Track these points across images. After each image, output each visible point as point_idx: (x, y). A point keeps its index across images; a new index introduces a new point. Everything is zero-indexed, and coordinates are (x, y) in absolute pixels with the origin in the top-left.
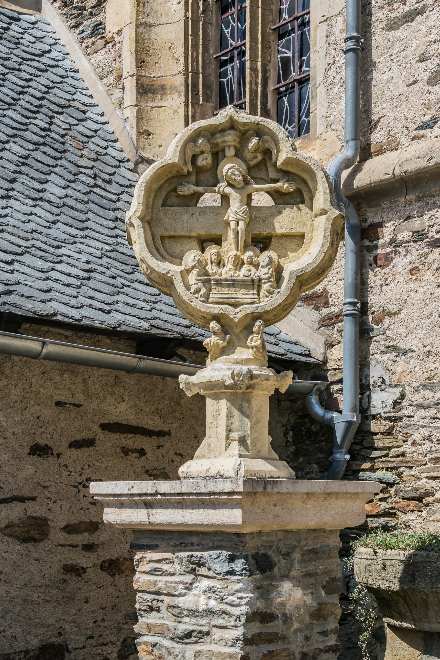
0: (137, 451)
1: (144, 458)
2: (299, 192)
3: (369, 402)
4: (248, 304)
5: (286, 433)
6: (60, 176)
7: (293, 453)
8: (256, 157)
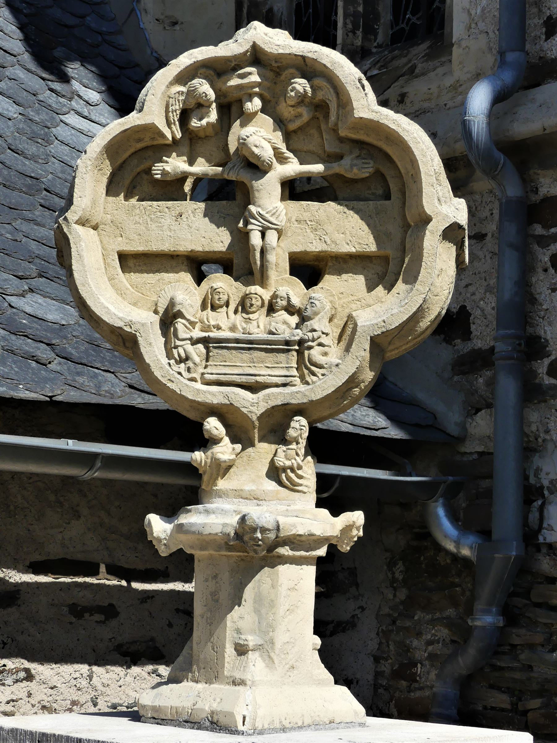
0: (100, 609)
1: (114, 623)
2: (379, 175)
3: (541, 519)
4: (277, 386)
5: (391, 565)
6: (8, 97)
7: (402, 603)
8: (300, 116)
